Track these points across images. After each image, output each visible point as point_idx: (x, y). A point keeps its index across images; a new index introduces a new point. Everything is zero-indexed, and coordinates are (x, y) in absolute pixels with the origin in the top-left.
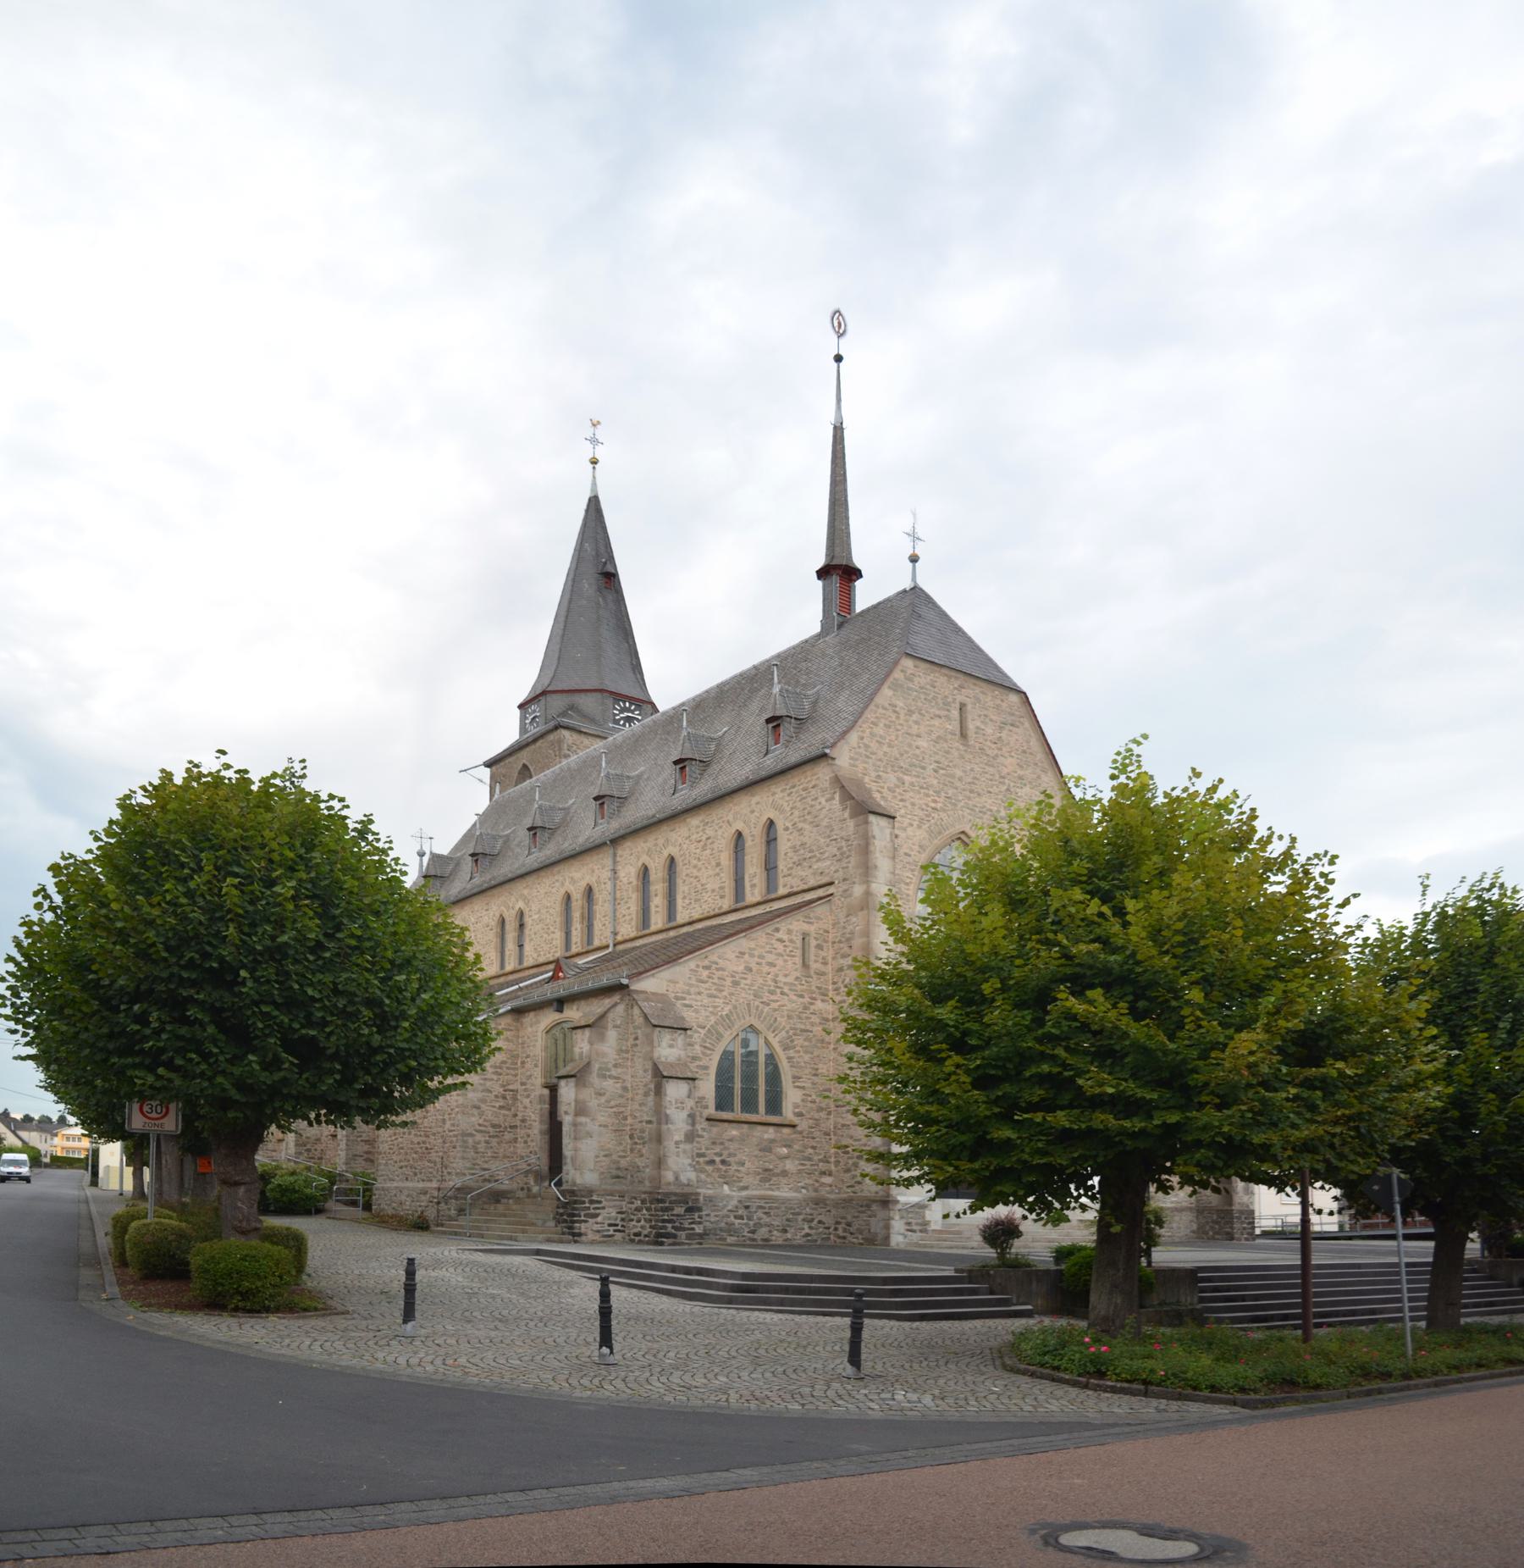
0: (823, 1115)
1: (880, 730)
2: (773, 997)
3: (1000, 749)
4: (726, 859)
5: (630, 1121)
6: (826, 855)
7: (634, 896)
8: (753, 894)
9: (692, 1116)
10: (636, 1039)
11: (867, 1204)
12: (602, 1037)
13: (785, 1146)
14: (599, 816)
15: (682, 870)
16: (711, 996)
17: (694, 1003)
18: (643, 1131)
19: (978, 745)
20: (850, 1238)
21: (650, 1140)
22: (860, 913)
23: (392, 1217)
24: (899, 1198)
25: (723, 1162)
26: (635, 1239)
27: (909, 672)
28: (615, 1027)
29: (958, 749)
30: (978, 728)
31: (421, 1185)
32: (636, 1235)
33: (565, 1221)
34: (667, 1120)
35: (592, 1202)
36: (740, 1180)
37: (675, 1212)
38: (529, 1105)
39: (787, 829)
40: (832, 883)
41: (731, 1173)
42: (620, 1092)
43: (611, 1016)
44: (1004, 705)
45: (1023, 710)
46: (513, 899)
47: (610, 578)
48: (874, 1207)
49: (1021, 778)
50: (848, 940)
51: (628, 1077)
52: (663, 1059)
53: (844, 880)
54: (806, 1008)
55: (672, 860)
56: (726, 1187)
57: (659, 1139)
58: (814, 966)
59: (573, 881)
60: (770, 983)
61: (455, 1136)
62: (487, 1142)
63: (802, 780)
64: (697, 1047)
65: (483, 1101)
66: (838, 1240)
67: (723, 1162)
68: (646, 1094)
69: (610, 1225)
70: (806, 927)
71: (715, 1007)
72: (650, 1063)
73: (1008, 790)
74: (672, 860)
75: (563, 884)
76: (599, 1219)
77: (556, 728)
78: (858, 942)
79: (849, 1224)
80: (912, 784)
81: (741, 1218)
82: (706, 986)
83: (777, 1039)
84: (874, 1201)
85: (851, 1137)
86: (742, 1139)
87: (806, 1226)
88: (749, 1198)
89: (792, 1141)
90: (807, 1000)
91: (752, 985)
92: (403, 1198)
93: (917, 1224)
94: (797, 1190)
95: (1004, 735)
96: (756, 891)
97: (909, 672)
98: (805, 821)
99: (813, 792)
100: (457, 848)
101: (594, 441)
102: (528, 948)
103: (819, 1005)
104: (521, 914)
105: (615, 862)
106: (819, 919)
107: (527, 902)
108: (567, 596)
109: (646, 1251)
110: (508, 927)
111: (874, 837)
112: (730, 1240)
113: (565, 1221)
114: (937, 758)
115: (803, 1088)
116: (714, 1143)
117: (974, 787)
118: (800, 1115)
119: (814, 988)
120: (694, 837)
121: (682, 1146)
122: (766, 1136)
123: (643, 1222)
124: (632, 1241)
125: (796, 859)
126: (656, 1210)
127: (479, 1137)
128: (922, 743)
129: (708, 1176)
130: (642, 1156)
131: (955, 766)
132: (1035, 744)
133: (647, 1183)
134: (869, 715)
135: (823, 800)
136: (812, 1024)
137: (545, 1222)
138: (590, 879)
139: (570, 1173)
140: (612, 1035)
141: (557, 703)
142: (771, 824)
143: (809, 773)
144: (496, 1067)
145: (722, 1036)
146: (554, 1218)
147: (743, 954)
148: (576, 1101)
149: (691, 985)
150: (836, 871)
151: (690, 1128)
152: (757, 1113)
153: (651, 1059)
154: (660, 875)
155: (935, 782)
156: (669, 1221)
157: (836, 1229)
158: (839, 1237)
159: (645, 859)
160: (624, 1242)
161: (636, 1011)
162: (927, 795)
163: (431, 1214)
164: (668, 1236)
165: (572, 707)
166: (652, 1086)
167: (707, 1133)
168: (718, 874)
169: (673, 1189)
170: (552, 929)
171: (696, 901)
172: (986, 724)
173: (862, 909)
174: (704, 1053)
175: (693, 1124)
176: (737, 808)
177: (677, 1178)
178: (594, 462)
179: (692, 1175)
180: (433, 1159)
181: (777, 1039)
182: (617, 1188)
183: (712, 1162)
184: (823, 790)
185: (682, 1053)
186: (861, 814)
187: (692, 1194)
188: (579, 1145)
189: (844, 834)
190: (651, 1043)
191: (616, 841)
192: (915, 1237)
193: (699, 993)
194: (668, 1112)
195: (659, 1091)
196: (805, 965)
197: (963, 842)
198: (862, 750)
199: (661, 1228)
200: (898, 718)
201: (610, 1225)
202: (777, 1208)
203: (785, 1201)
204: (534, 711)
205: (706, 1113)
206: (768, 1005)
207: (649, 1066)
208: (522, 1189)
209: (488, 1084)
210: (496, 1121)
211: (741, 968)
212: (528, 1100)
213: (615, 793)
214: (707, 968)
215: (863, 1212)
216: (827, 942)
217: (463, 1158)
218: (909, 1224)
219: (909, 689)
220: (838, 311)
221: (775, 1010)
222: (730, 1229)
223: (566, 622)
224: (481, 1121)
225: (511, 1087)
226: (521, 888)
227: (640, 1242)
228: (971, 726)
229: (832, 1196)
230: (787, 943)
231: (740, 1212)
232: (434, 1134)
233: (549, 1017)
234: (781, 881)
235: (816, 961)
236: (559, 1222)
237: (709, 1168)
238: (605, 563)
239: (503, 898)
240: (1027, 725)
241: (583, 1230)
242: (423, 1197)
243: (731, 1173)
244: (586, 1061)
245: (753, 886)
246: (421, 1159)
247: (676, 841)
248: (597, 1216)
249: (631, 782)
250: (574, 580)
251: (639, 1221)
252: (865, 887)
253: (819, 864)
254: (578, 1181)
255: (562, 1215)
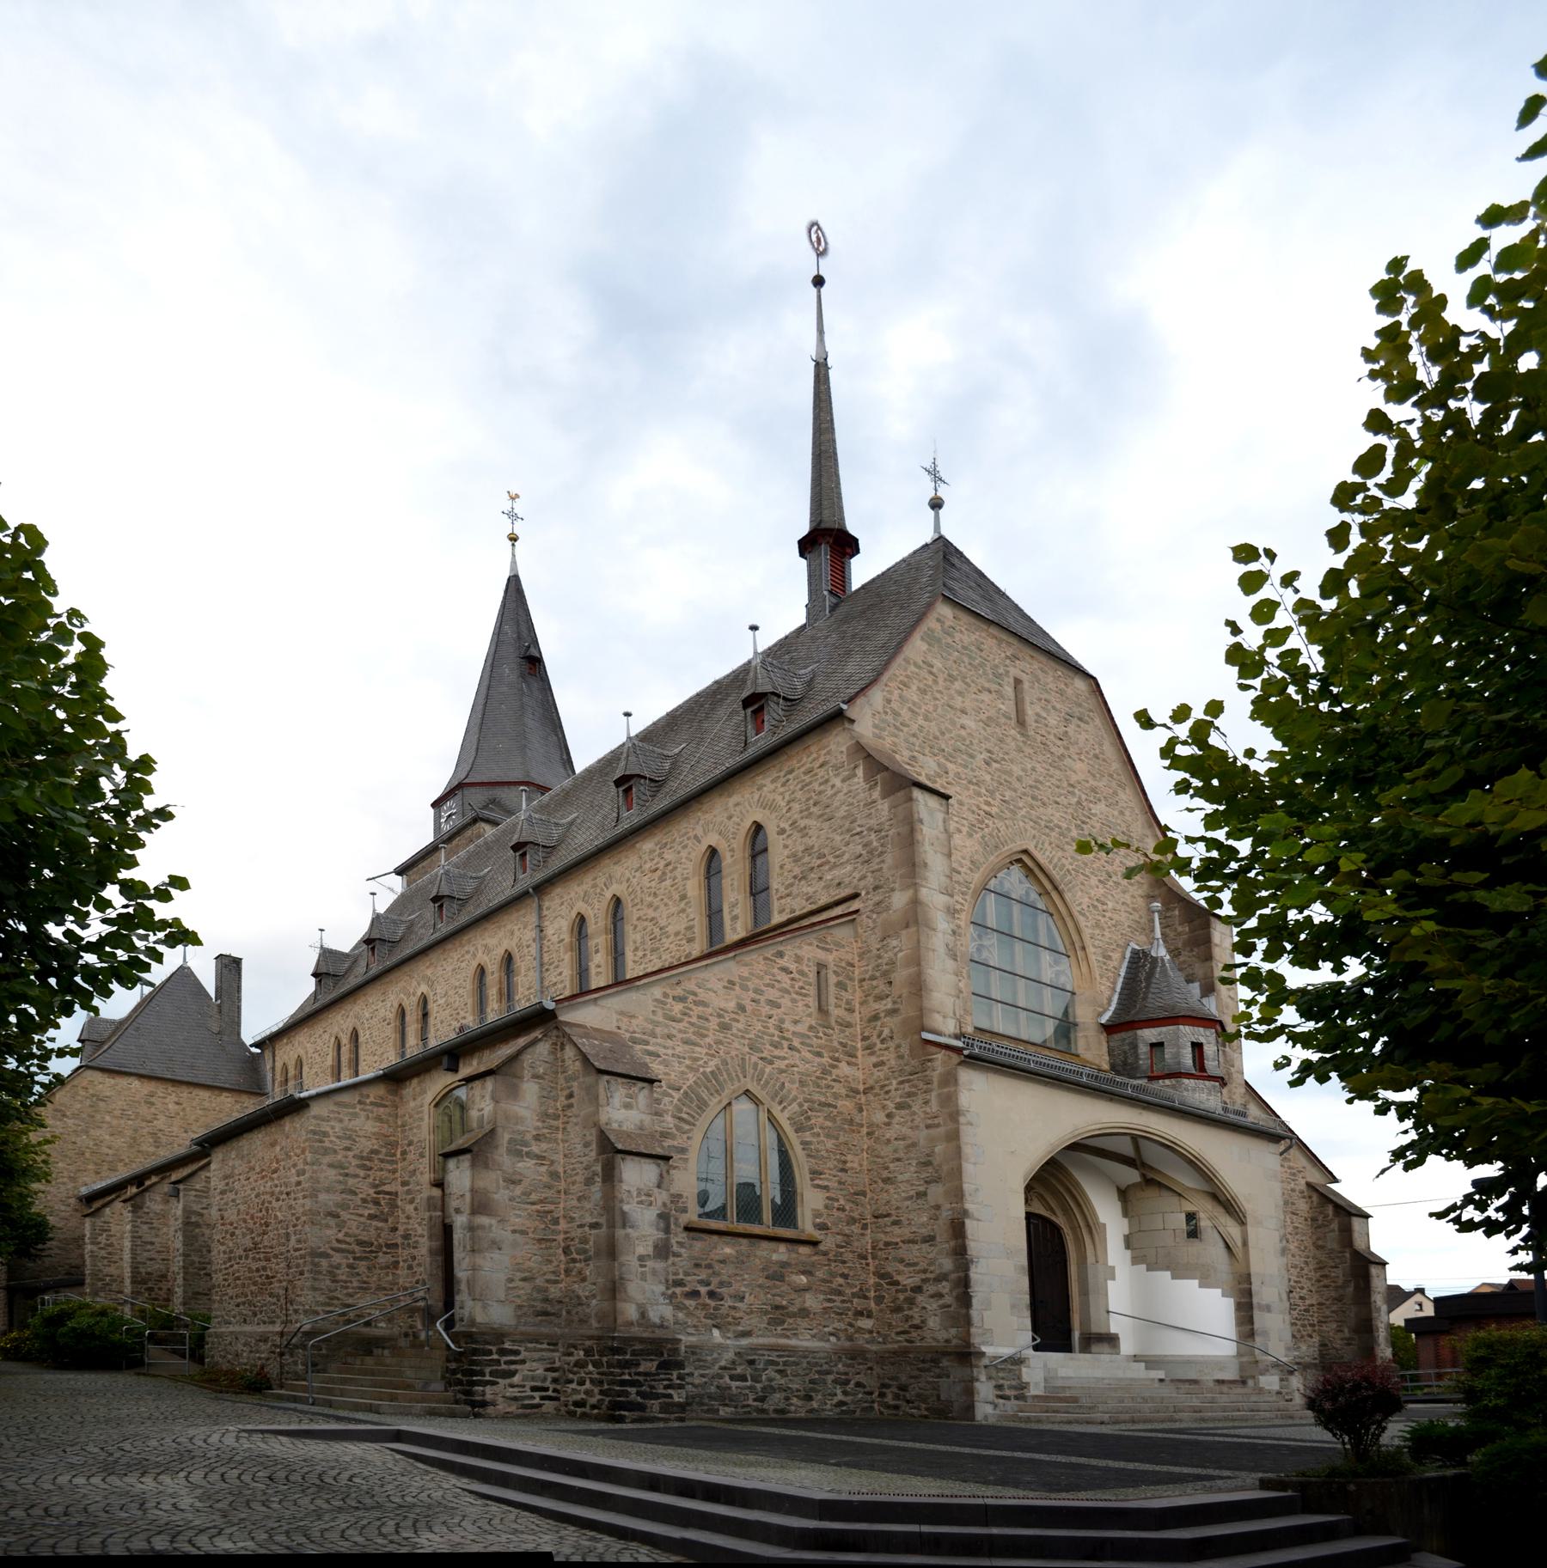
0: (856, 1229)
1: (912, 694)
2: (777, 1053)
3: (1068, 749)
4: (694, 888)
5: (563, 1225)
6: (846, 857)
7: (567, 957)
8: (734, 930)
9: (664, 1217)
10: (571, 1096)
11: (935, 1356)
12: (514, 1093)
13: (803, 1273)
14: (519, 871)
15: (631, 912)
16: (686, 1042)
17: (661, 1051)
18: (584, 1241)
19: (1039, 738)
20: (906, 1408)
21: (597, 1254)
22: (904, 932)
23: (227, 1373)
24: (984, 1349)
25: (711, 1294)
26: (576, 1412)
27: (948, 623)
28: (536, 1076)
29: (1014, 739)
30: (1038, 715)
31: (262, 1328)
32: (577, 1404)
33: (460, 1383)
34: (625, 1221)
35: (503, 1352)
36: (737, 1323)
37: (641, 1369)
38: (413, 1214)
39: (782, 832)
40: (855, 896)
41: (724, 1311)
42: (546, 1179)
43: (527, 1059)
44: (1069, 691)
45: (1092, 703)
46: (414, 983)
47: (533, 663)
48: (945, 1363)
49: (1094, 790)
50: (885, 974)
51: (559, 1158)
52: (615, 1126)
53: (876, 888)
54: (825, 1072)
55: (617, 902)
56: (716, 1332)
57: (611, 1251)
58: (836, 1012)
59: (486, 948)
60: (772, 1030)
61: (302, 1257)
62: (350, 1266)
63: (803, 760)
64: (669, 1118)
65: (344, 1206)
66: (885, 1411)
67: (711, 1294)
68: (589, 1182)
69: (534, 1389)
70: (821, 955)
71: (696, 1059)
72: (594, 1131)
73: (1079, 803)
74: (617, 902)
75: (474, 955)
76: (516, 1379)
77: (475, 821)
78: (901, 975)
79: (903, 1388)
80: (958, 775)
81: (743, 1378)
82: (680, 1026)
83: (786, 1114)
84: (945, 1354)
85: (902, 1261)
86: (740, 1261)
87: (839, 1391)
88: (754, 1349)
89: (813, 1264)
90: (826, 1060)
91: (747, 1031)
92: (240, 1347)
93: (1010, 1387)
94: (823, 1337)
95: (1071, 729)
96: (739, 925)
97: (948, 623)
98: (810, 816)
99: (822, 772)
100: (353, 949)
101: (513, 516)
102: (431, 1034)
103: (844, 1069)
104: (424, 1001)
105: (540, 917)
106: (839, 945)
107: (431, 983)
108: (486, 683)
109: (595, 1433)
110: (408, 1018)
111: (921, 821)
112: (724, 1412)
113: (460, 1383)
114: (989, 746)
115: (826, 1188)
116: (697, 1265)
117: (1036, 792)
118: (822, 1227)
119: (835, 1044)
120: (647, 866)
121: (650, 1264)
122: (775, 1257)
123: (588, 1385)
124: (572, 1414)
125: (797, 871)
126: (610, 1365)
127: (337, 1258)
128: (969, 722)
129: (689, 1314)
130: (584, 1280)
131: (1012, 761)
132: (1109, 750)
133: (595, 1324)
134: (897, 668)
135: (837, 782)
136: (836, 1096)
137: (427, 1384)
138: (508, 944)
139: (468, 1308)
140: (530, 1090)
141: (477, 797)
142: (758, 828)
143: (813, 749)
144: (362, 1158)
145: (706, 1104)
146: (443, 1377)
147: (732, 983)
148: (472, 1190)
149: (657, 1024)
150: (863, 877)
151: (661, 1235)
152: (760, 1222)
153: (596, 1124)
154: (601, 924)
155: (988, 778)
156: (632, 1383)
157: (882, 1395)
158: (888, 1407)
159: (580, 907)
160: (558, 1416)
161: (569, 1052)
162: (979, 794)
163: (273, 1370)
164: (631, 1406)
165: (493, 801)
166: (598, 1168)
167: (687, 1250)
168: (683, 911)
169: (636, 1331)
170: (462, 1014)
171: (653, 950)
172: (1048, 712)
173: (907, 926)
174: (678, 1128)
175: (667, 1230)
176: (708, 817)
177: (643, 1315)
178: (513, 539)
179: (667, 1311)
180: (276, 1291)
181: (786, 1114)
182: (544, 1330)
183: (695, 1294)
184: (836, 768)
185: (647, 1119)
186: (899, 790)
187: (667, 1340)
188: (479, 1260)
189: (873, 822)
190: (594, 1100)
191: (541, 889)
192: (1011, 1406)
193: (670, 1037)
194: (626, 1208)
195: (610, 1175)
196: (822, 1010)
197: (1025, 866)
198: (889, 718)
199: (620, 1394)
200: (935, 682)
201: (534, 1389)
202: (797, 1364)
203: (807, 1353)
204: (451, 808)
205: (684, 1219)
206: (771, 1063)
207: (592, 1136)
208: (406, 1335)
209: (351, 1181)
210: (364, 1237)
211: (731, 1005)
212: (411, 1207)
213: (540, 841)
214: (682, 999)
215: (928, 1370)
216: (852, 979)
217: (314, 1289)
218: (999, 1387)
219: (948, 645)
220: (814, 224)
221: (782, 1071)
222: (724, 1397)
223: (484, 709)
224: (340, 1236)
225: (386, 1188)
226: (424, 968)
227: (584, 1416)
228: (1030, 712)
229: (874, 1348)
230: (795, 975)
231: (739, 1370)
232: (276, 1256)
233: (440, 1081)
234: (776, 905)
235: (837, 1006)
236: (449, 1384)
237: (691, 1303)
238: (529, 647)
239: (402, 984)
240: (1098, 721)
241: (488, 1397)
242: (263, 1346)
243: (724, 1311)
244: (488, 1128)
245: (735, 918)
246: (261, 1291)
247: (623, 875)
248: (513, 1374)
249: (560, 830)
250: (492, 666)
251: (582, 1383)
252: (910, 892)
253: (836, 872)
254: (479, 1319)
255: (454, 1372)
